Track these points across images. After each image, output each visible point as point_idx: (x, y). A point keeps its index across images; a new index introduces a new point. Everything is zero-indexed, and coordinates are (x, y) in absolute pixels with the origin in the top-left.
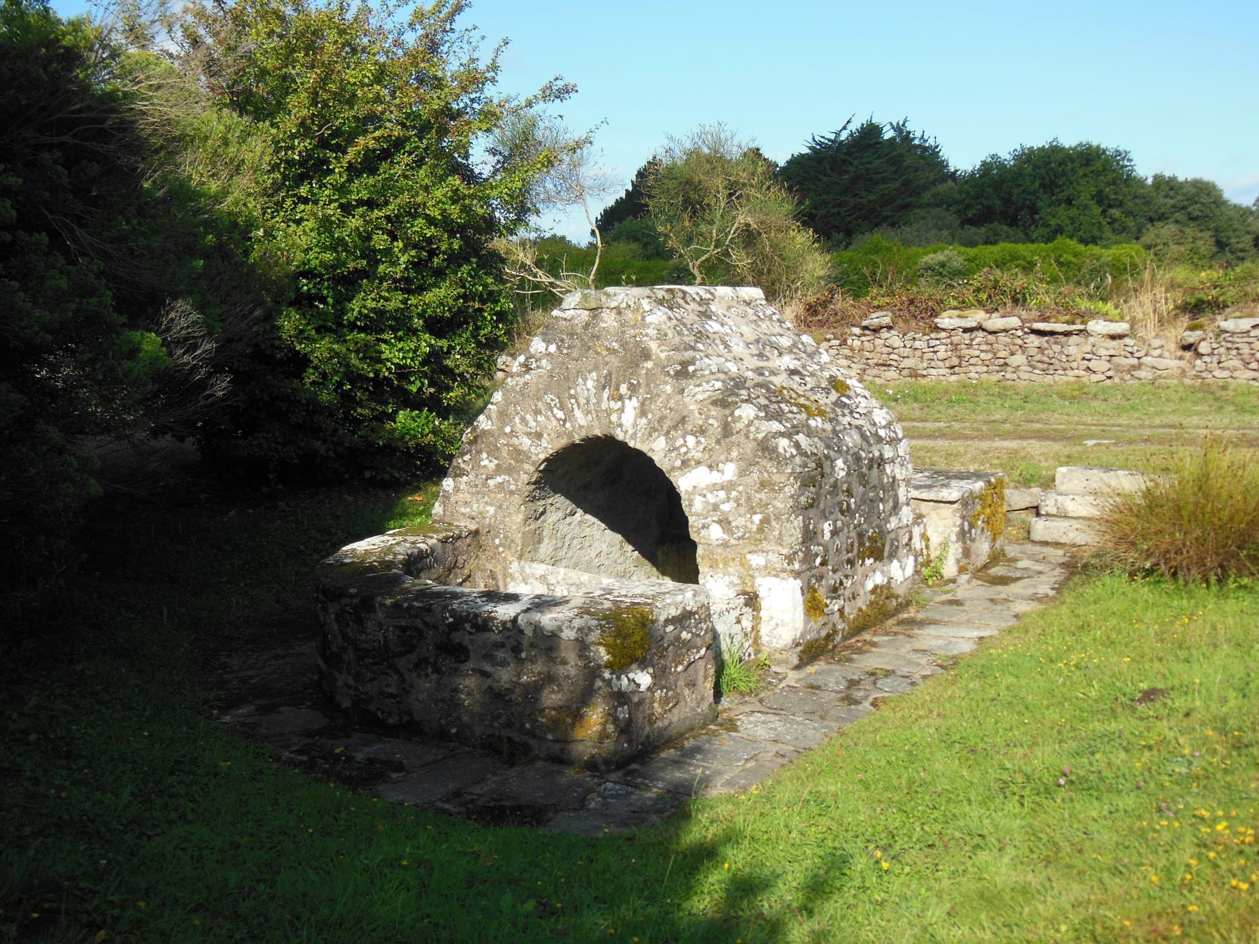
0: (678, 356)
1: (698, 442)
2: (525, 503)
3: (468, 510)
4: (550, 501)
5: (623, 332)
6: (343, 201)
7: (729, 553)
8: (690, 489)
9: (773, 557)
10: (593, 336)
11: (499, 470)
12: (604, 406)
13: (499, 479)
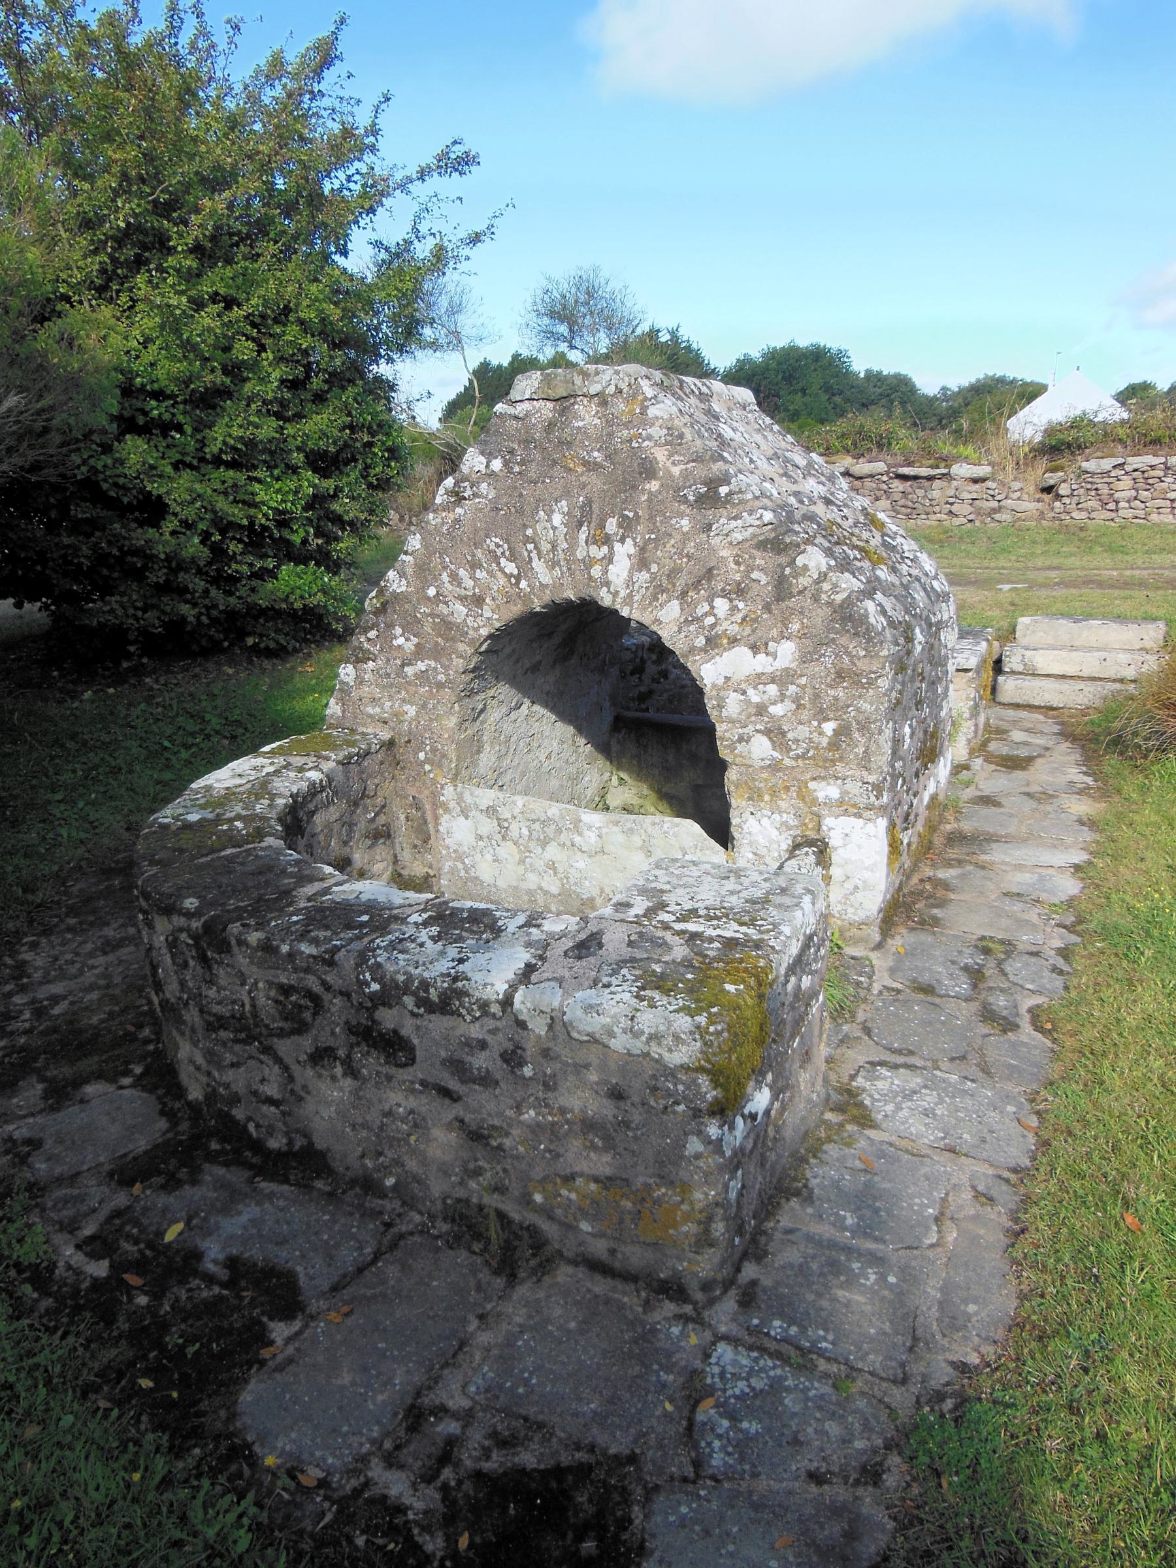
0: (701, 471)
1: (734, 609)
2: (460, 700)
3: (378, 710)
4: (492, 692)
5: (610, 435)
6: (193, 293)
7: (778, 779)
8: (720, 681)
9: (854, 788)
10: (561, 443)
11: (420, 652)
12: (580, 554)
13: (421, 666)
